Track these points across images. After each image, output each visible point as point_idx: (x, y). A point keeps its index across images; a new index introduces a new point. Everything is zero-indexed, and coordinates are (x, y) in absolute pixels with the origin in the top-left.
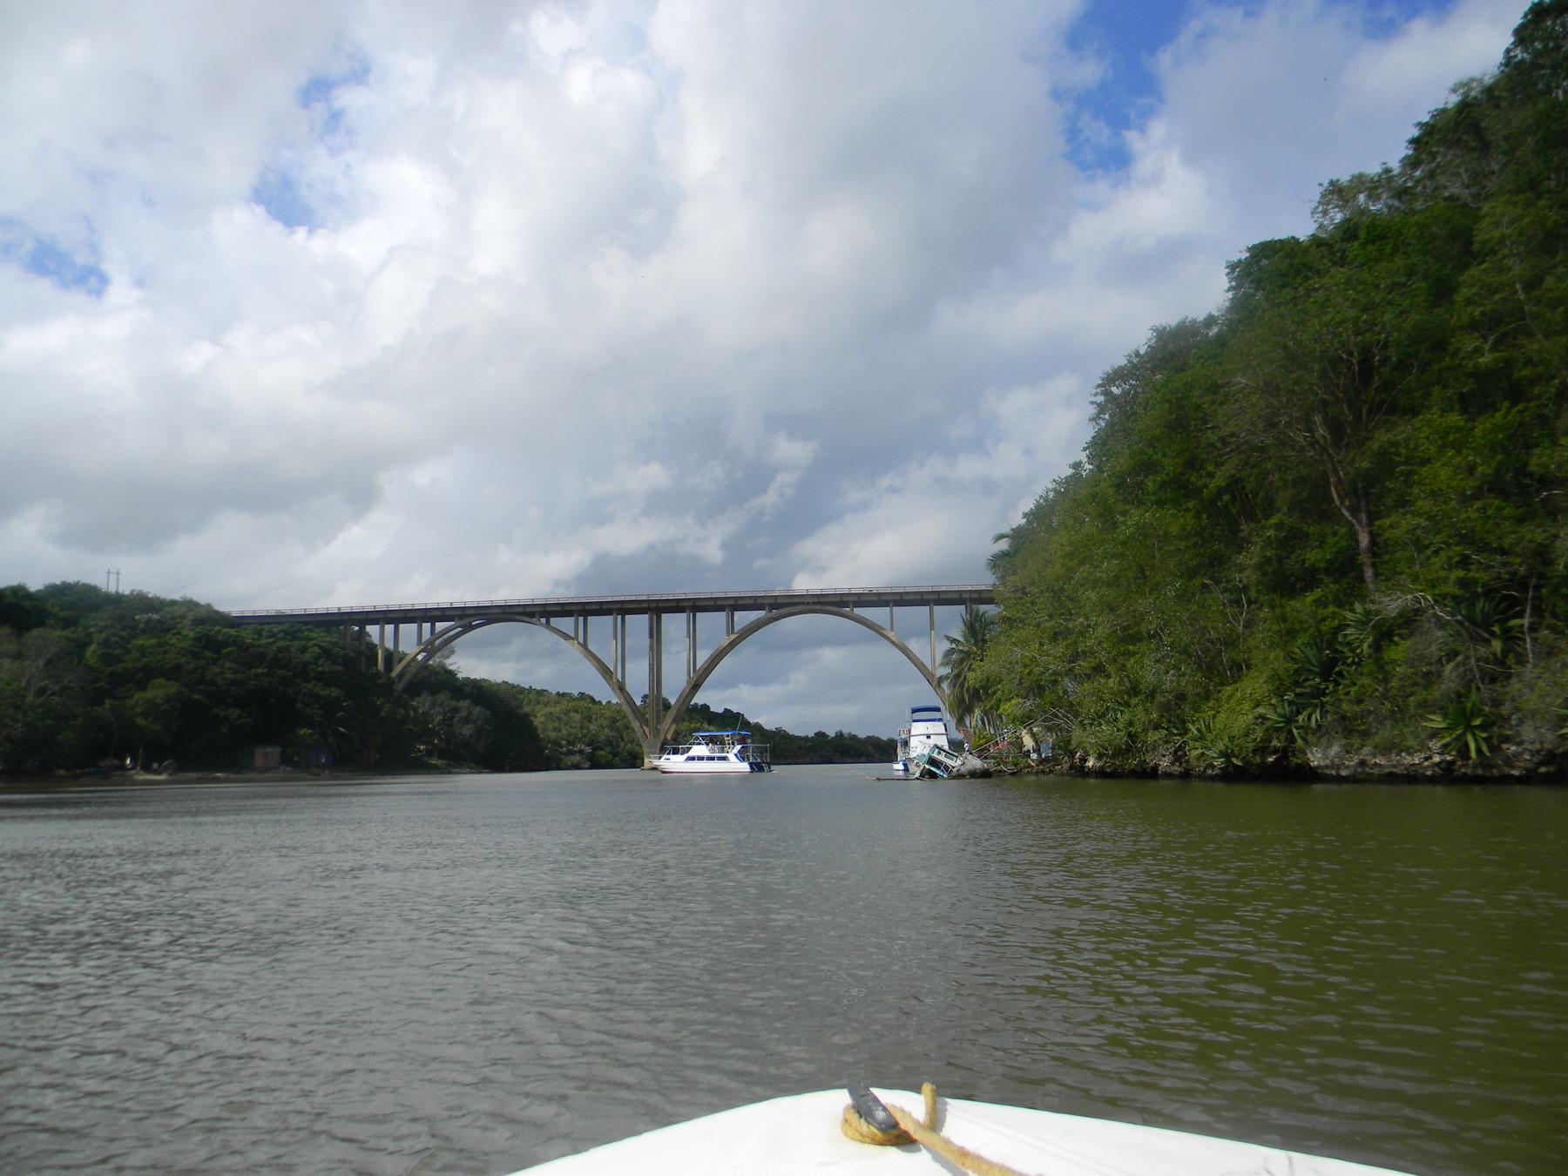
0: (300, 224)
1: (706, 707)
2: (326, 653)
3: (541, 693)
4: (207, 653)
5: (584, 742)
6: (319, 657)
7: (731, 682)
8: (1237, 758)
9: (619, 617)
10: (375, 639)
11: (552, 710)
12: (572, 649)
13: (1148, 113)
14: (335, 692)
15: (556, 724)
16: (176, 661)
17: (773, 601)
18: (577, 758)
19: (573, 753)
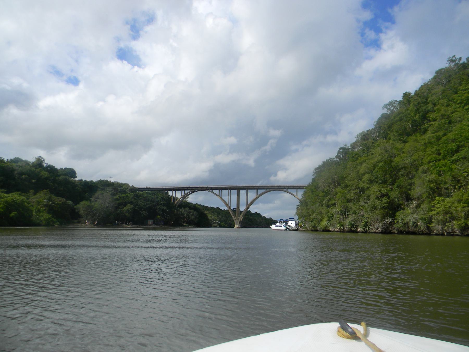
12: (218, 198)
14: (165, 208)
18: (216, 224)
19: (215, 223)
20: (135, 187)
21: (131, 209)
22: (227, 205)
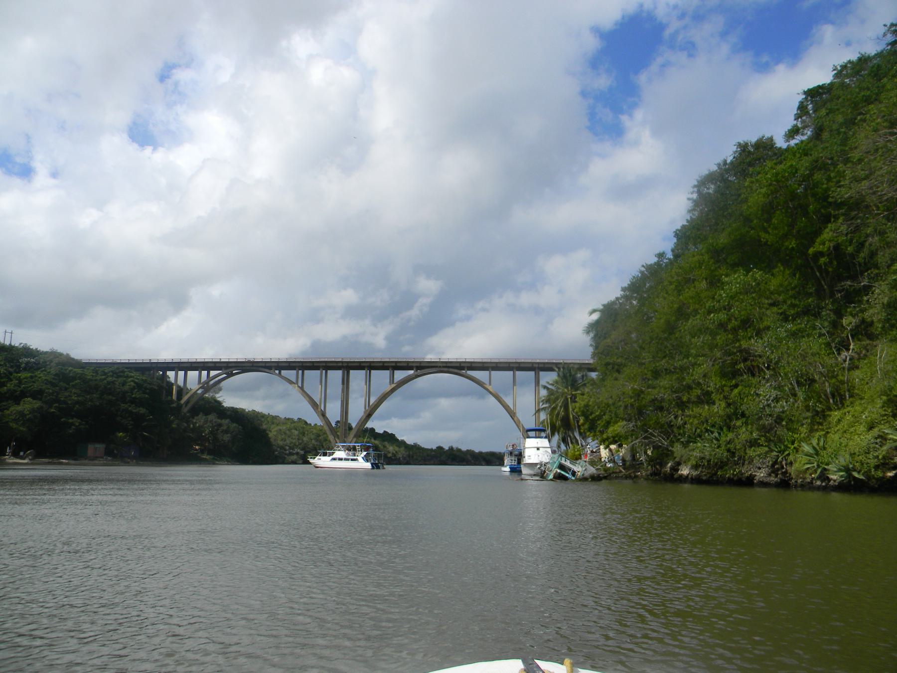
0: (148, 145)
1: (373, 430)
2: (139, 386)
3: (276, 417)
4: (61, 384)
6: (134, 388)
7: (383, 418)
8: (859, 472)
9: (324, 371)
10: (172, 380)
11: (281, 428)
12: (294, 391)
13: (634, 106)
14: (142, 410)
16: (40, 387)
17: (418, 365)
18: (294, 457)
19: (293, 454)
20: (73, 359)
21: (33, 411)
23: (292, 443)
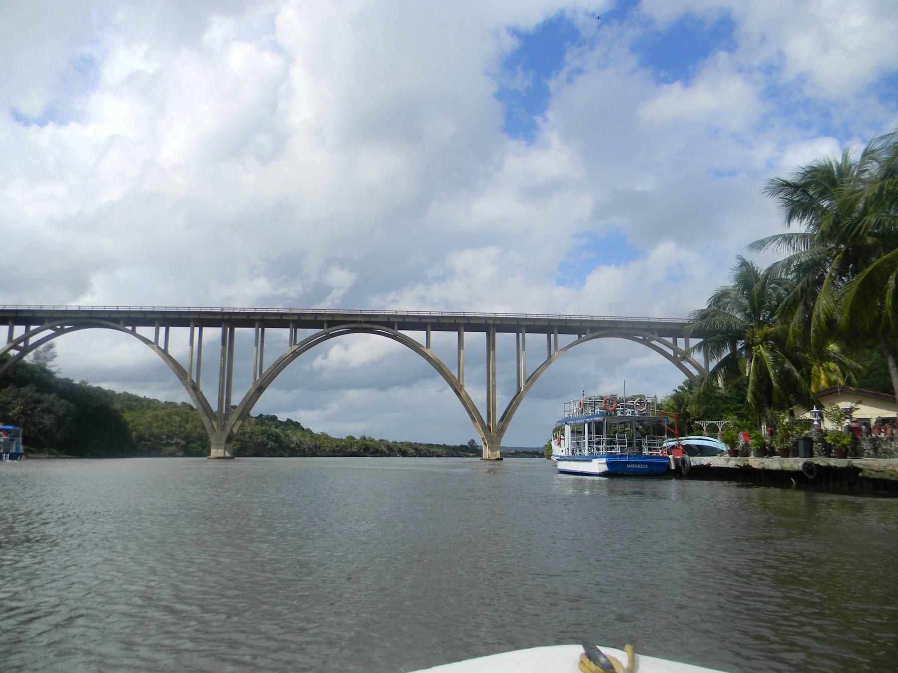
5: (180, 437)
15: (160, 423)
17: (330, 319)
19: (171, 445)
22: (185, 378)
23: (171, 431)
